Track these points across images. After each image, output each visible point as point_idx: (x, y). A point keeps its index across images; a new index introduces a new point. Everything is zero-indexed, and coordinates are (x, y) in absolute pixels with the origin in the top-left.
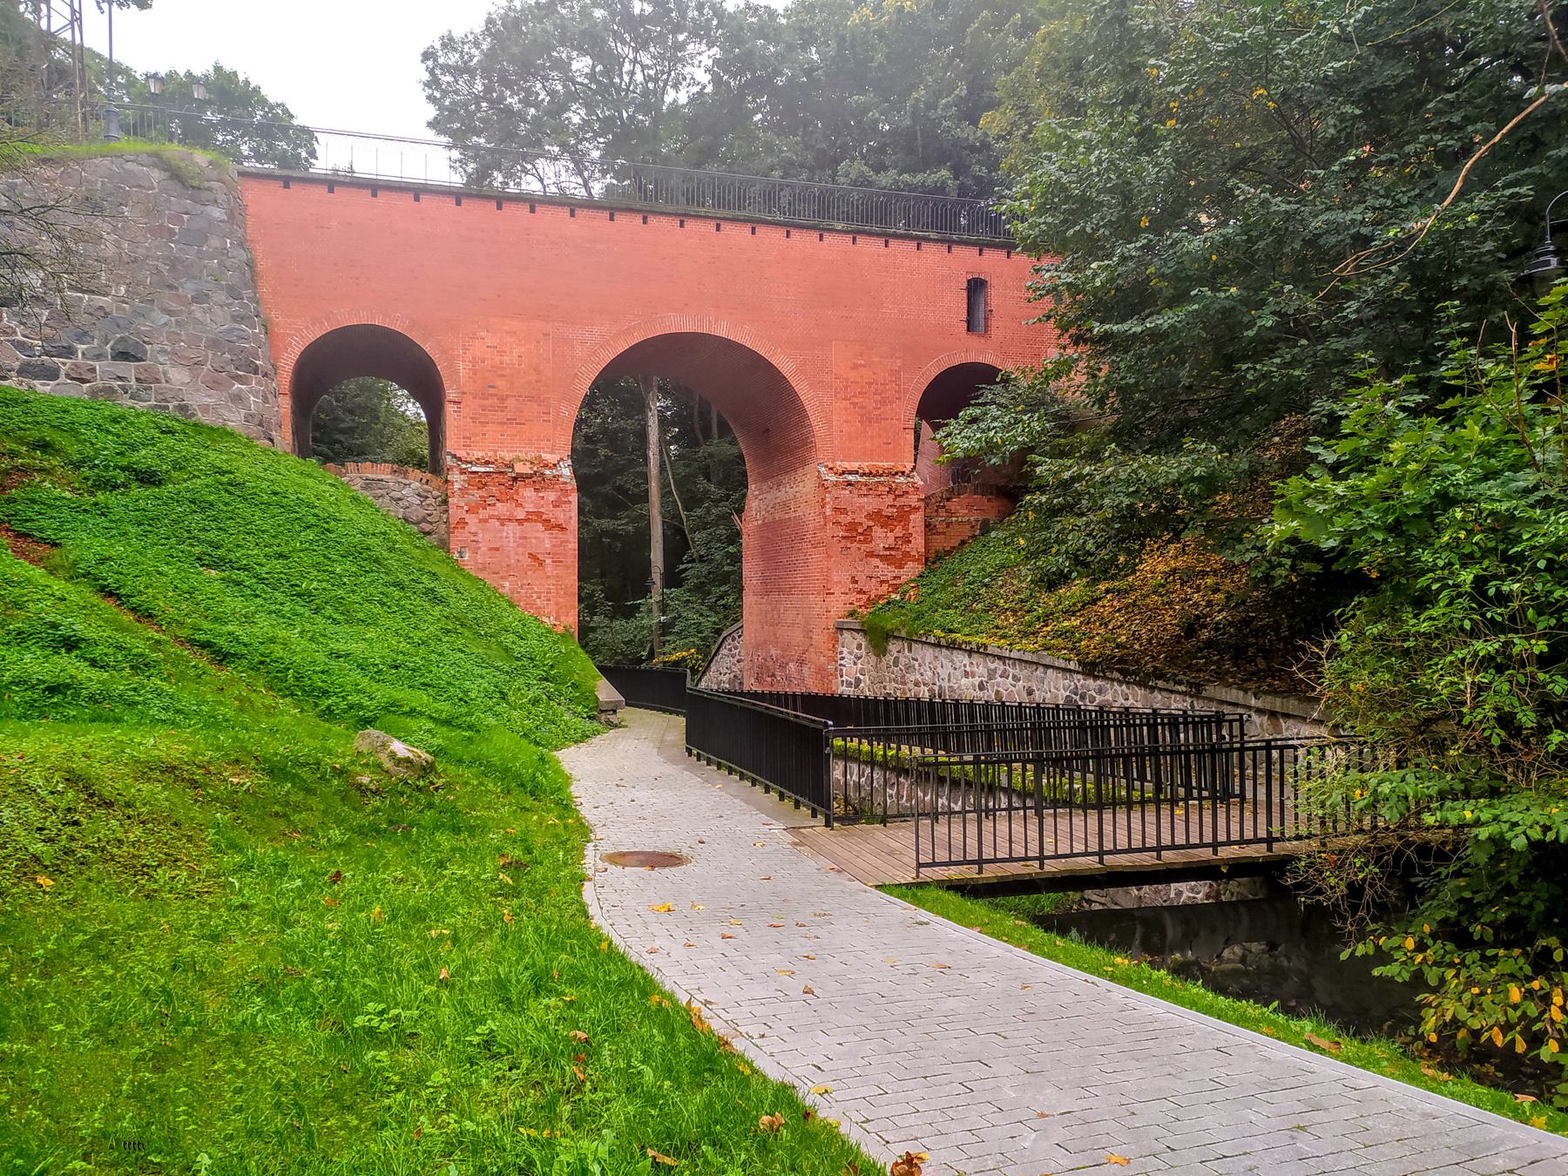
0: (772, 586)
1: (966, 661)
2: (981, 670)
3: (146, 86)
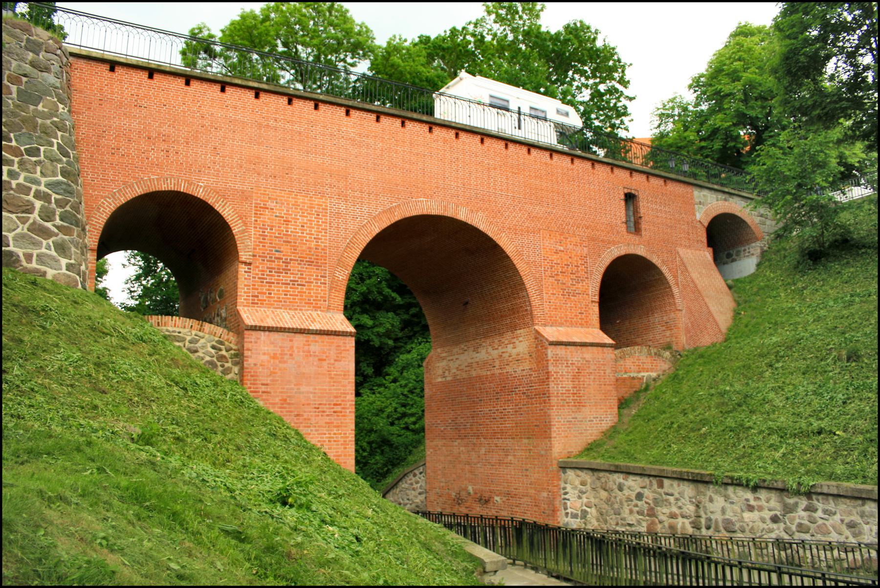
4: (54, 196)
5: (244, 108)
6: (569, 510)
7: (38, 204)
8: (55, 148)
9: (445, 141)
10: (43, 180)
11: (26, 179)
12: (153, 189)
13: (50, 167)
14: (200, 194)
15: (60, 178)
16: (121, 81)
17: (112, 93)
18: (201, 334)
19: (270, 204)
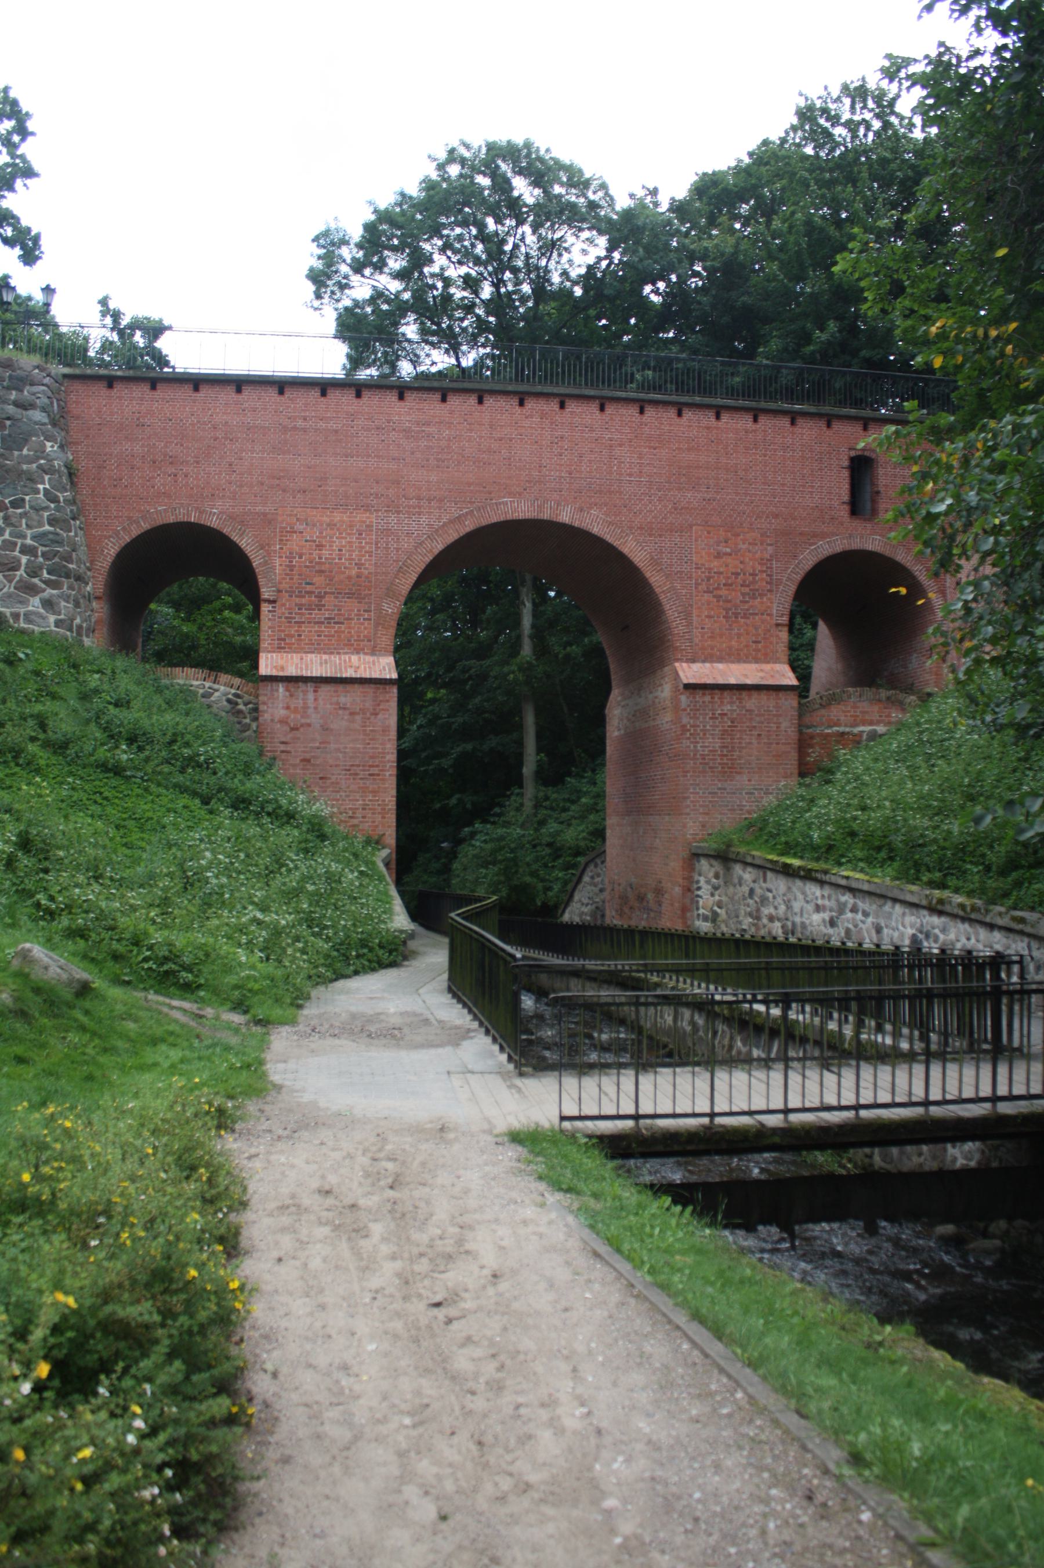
0: (638, 807)
1: (818, 892)
2: (832, 903)
3: (446, 179)
4: (41, 549)
5: (265, 409)
6: (701, 911)
7: (24, 559)
8: (41, 496)
9: (543, 415)
10: (29, 533)
11: (11, 535)
12: (160, 522)
13: (36, 517)
14: (214, 522)
15: (47, 528)
16: (120, 398)
17: (112, 414)
18: (216, 686)
19: (299, 527)
